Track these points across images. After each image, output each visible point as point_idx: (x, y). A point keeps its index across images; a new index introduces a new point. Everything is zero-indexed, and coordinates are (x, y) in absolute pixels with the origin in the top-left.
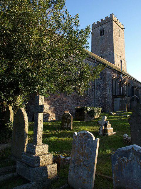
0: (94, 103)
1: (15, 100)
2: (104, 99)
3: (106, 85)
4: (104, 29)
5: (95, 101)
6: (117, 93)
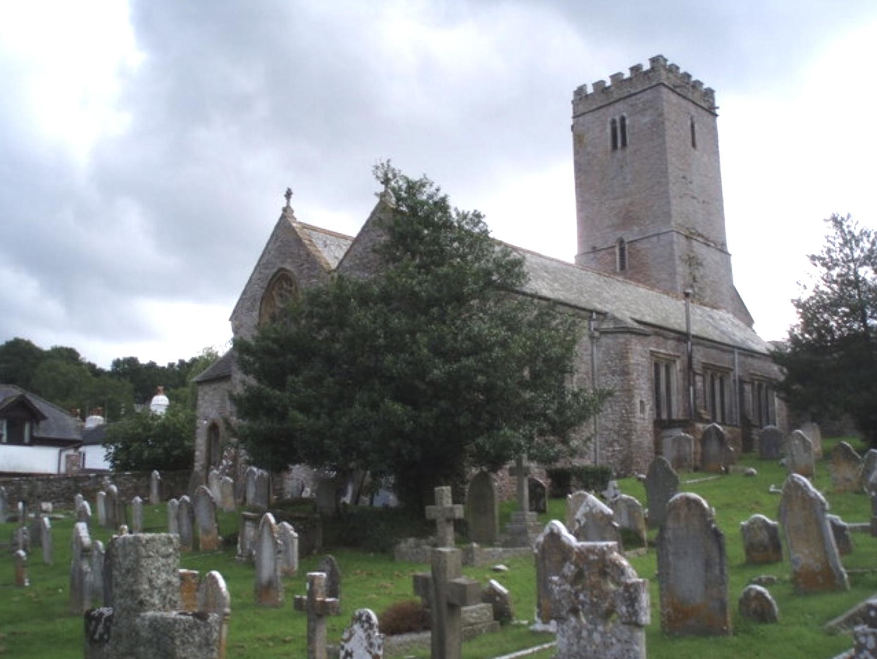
0: (595, 451)
1: (382, 473)
2: (627, 437)
3: (629, 392)
4: (627, 122)
5: (598, 443)
6: (674, 408)
